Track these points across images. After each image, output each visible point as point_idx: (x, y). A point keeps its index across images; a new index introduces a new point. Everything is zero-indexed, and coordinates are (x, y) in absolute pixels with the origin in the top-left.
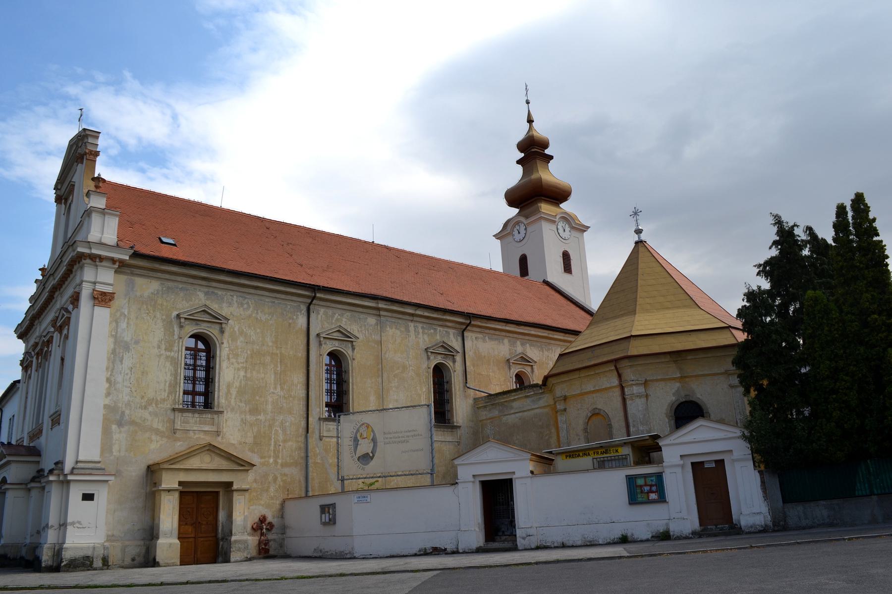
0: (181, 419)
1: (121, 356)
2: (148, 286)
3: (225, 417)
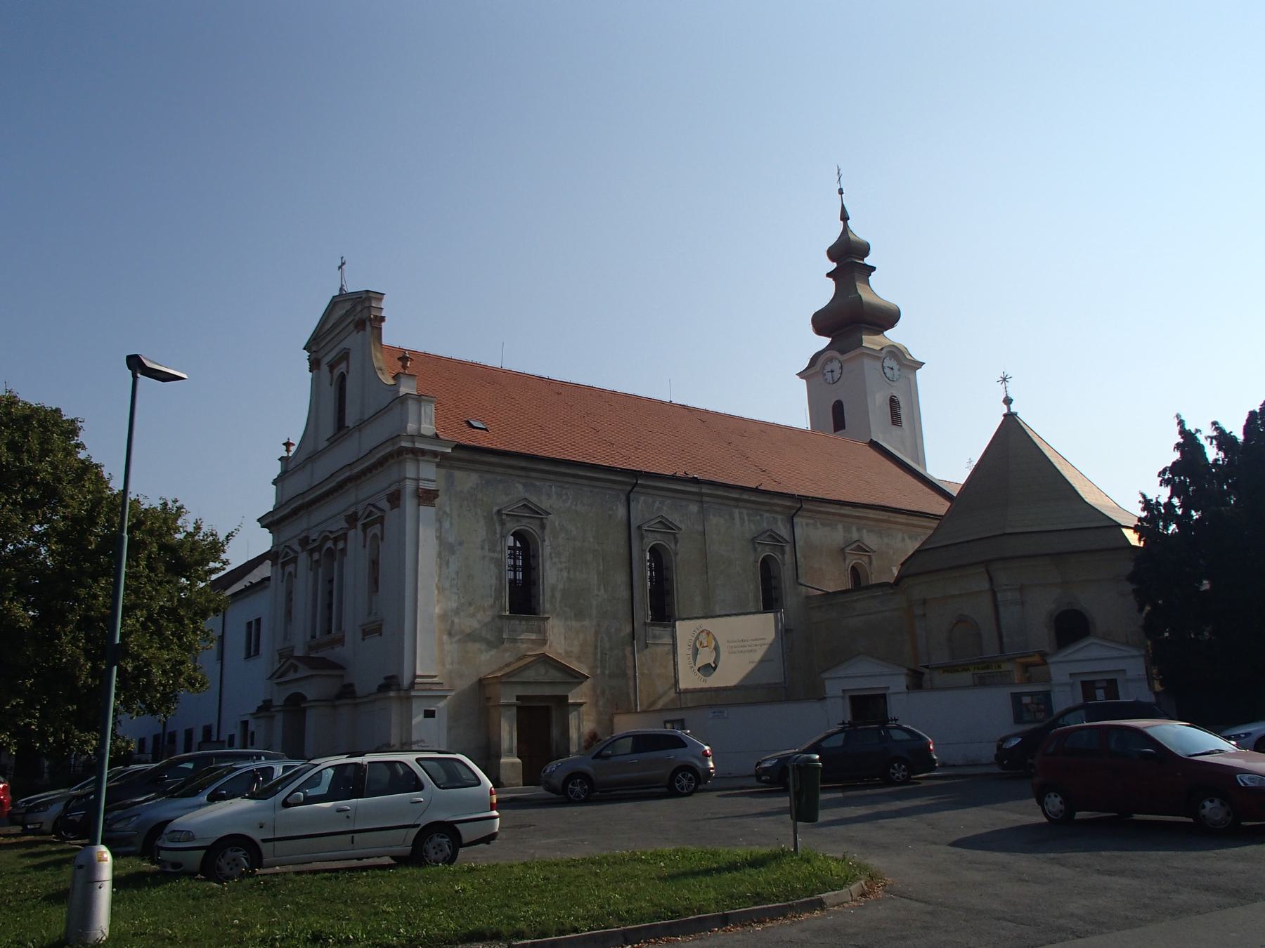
2: (467, 480)
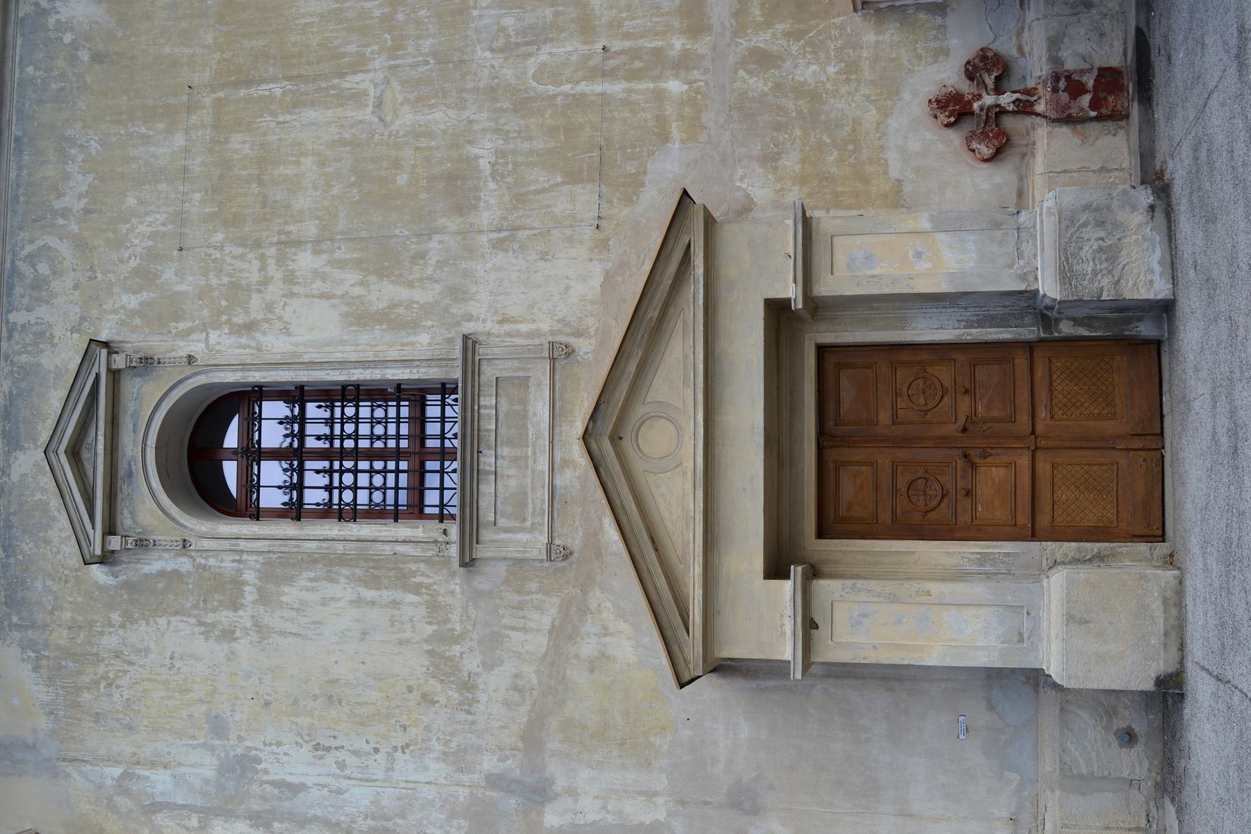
0: (507, 530)
1: (276, 791)
3: (489, 325)
